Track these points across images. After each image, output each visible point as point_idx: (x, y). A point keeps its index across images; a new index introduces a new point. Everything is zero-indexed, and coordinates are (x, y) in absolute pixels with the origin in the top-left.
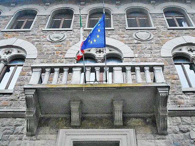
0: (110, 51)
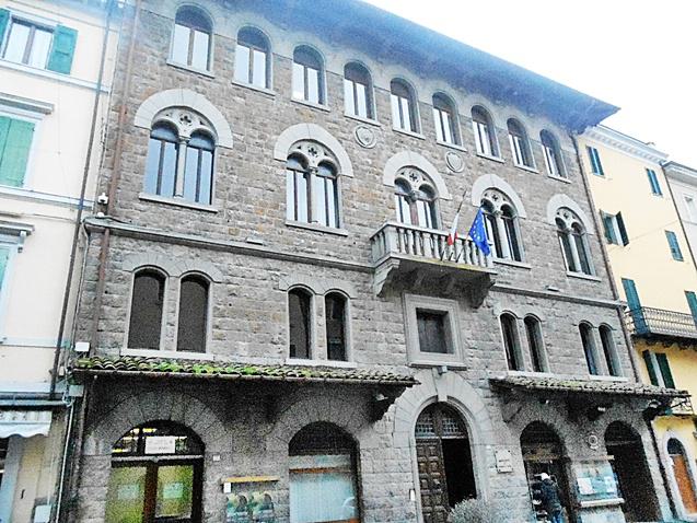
0: (201, 123)
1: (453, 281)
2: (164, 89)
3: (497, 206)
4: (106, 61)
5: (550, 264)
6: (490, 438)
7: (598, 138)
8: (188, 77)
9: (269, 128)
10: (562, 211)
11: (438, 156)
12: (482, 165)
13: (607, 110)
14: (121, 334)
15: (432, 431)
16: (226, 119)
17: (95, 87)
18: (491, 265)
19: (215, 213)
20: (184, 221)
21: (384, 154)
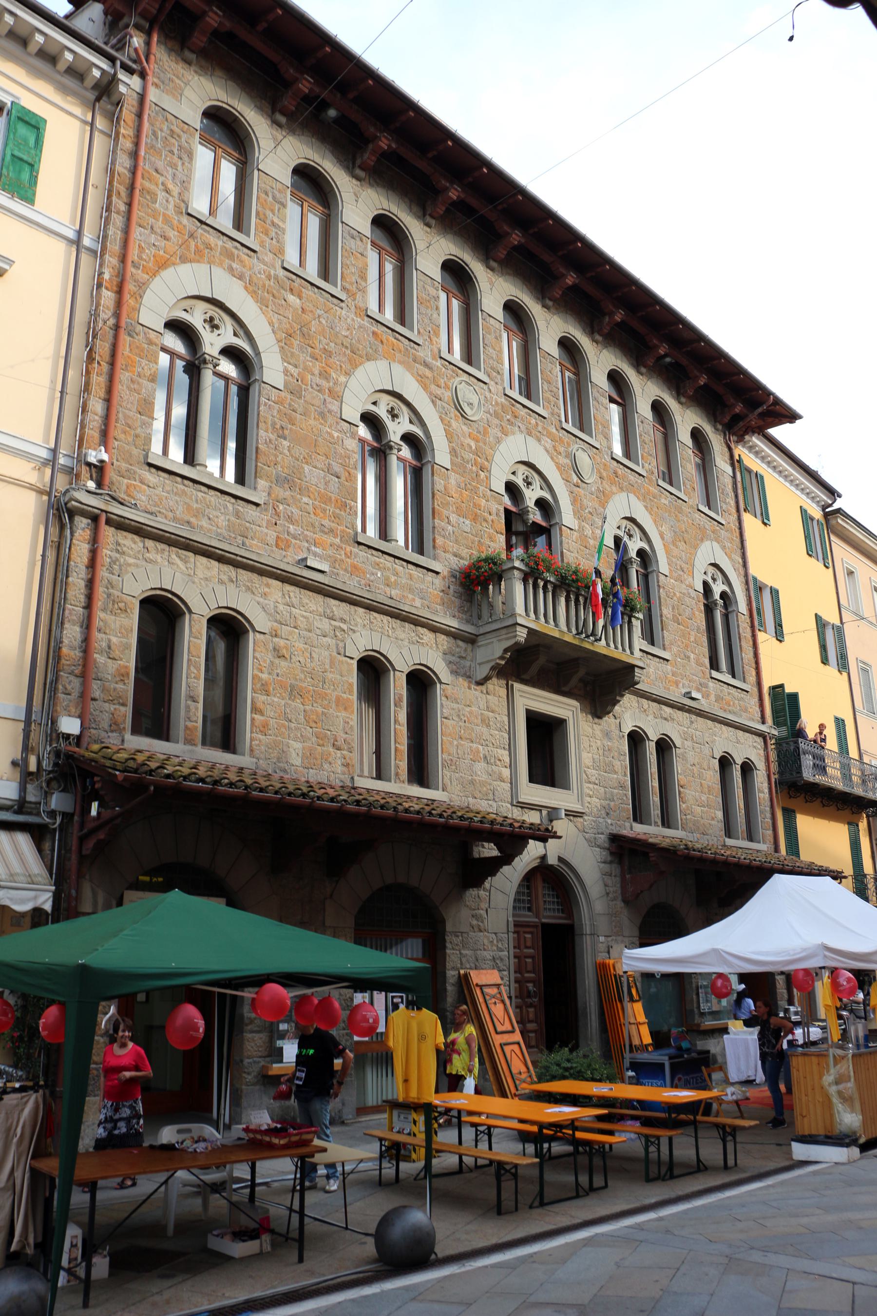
1: (581, 672)
2: (184, 260)
3: (634, 546)
4: (91, 189)
5: (692, 656)
6: (603, 925)
7: (757, 454)
8: (220, 243)
9: (335, 360)
10: (385, 399)
11: (562, 449)
12: (506, 418)
13: (786, 415)
14: (123, 709)
15: (529, 909)
16: (274, 332)
17: (71, 235)
18: (637, 653)
19: (257, 505)
20: (213, 514)
21: (494, 432)
